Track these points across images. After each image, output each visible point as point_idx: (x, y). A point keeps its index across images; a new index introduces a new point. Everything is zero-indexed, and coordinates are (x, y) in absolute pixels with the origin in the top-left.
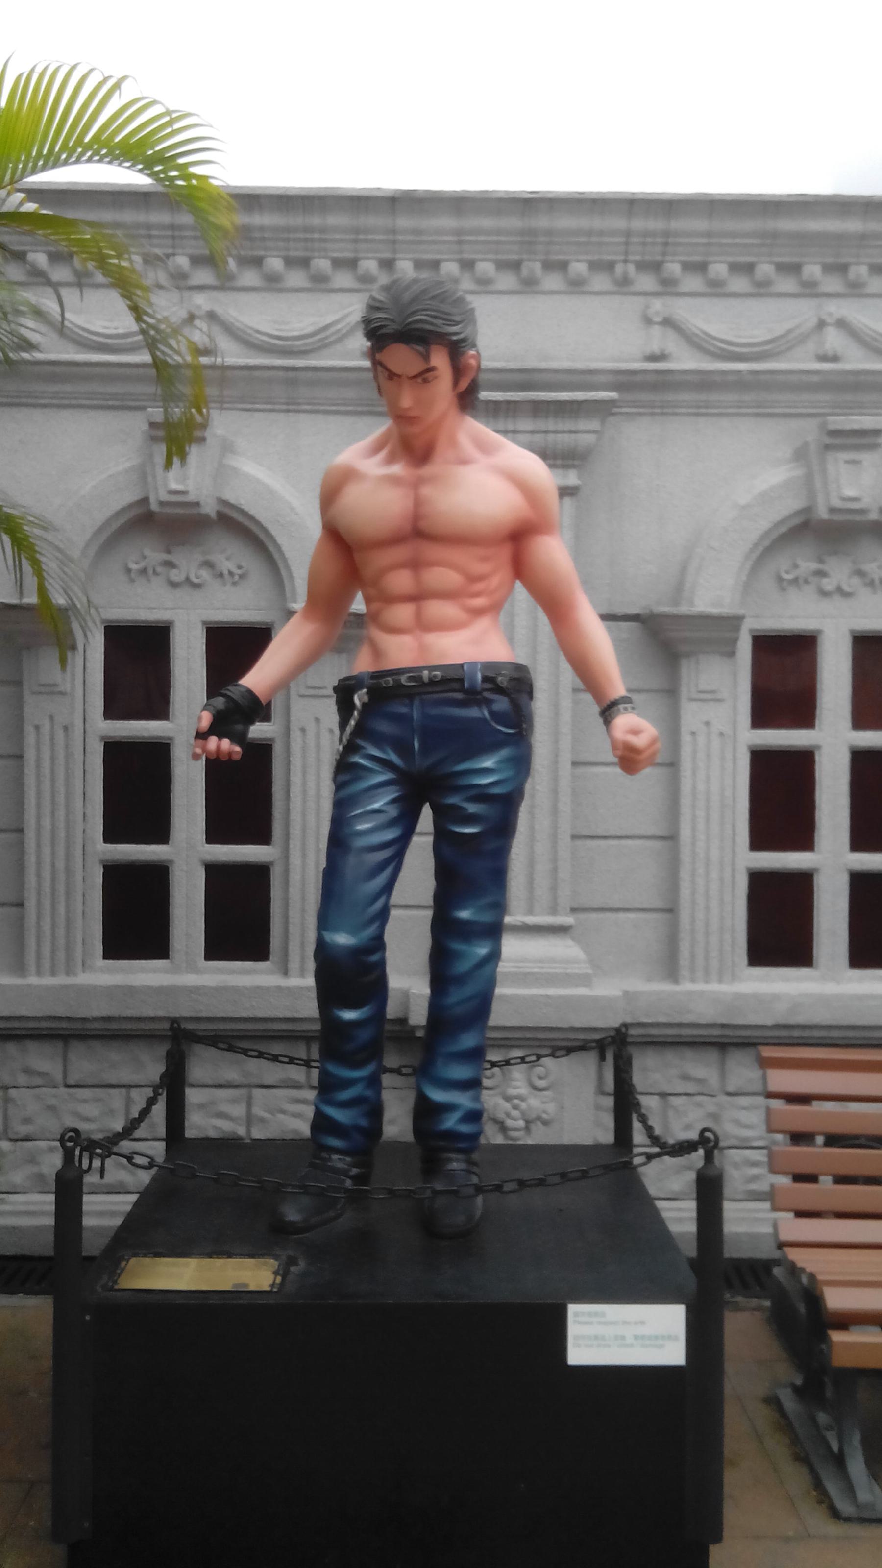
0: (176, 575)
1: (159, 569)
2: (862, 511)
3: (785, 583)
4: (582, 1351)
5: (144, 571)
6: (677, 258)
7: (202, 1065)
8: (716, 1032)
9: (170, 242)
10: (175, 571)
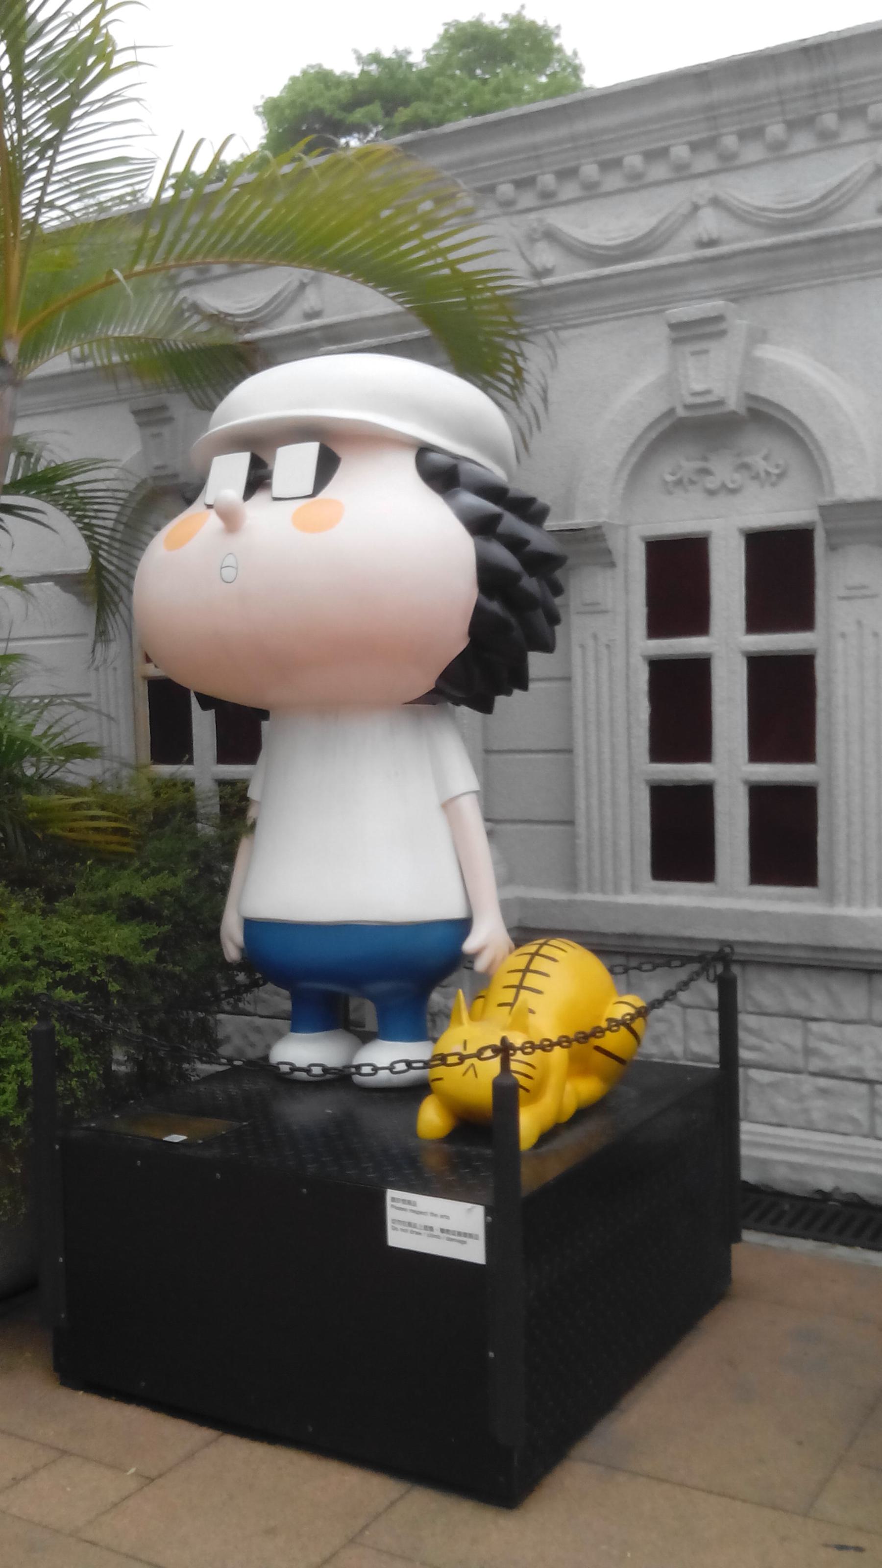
0: (711, 483)
1: (695, 478)
4: (396, 1239)
5: (679, 483)
7: (757, 991)
8: (675, 945)
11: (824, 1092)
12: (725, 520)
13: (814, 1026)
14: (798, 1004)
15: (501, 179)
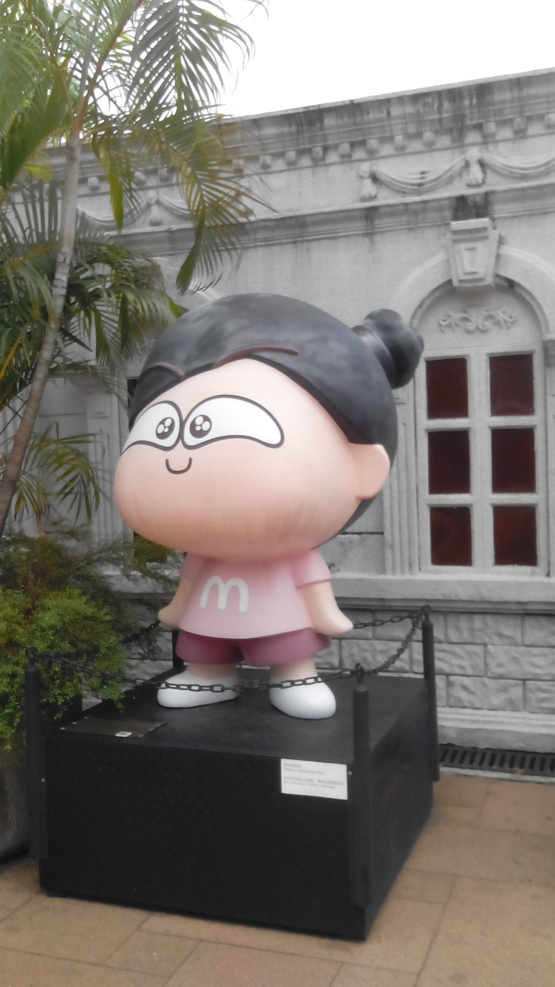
0: (471, 326)
1: (459, 323)
2: (482, 280)
4: (289, 787)
5: (449, 326)
9: (546, 105)
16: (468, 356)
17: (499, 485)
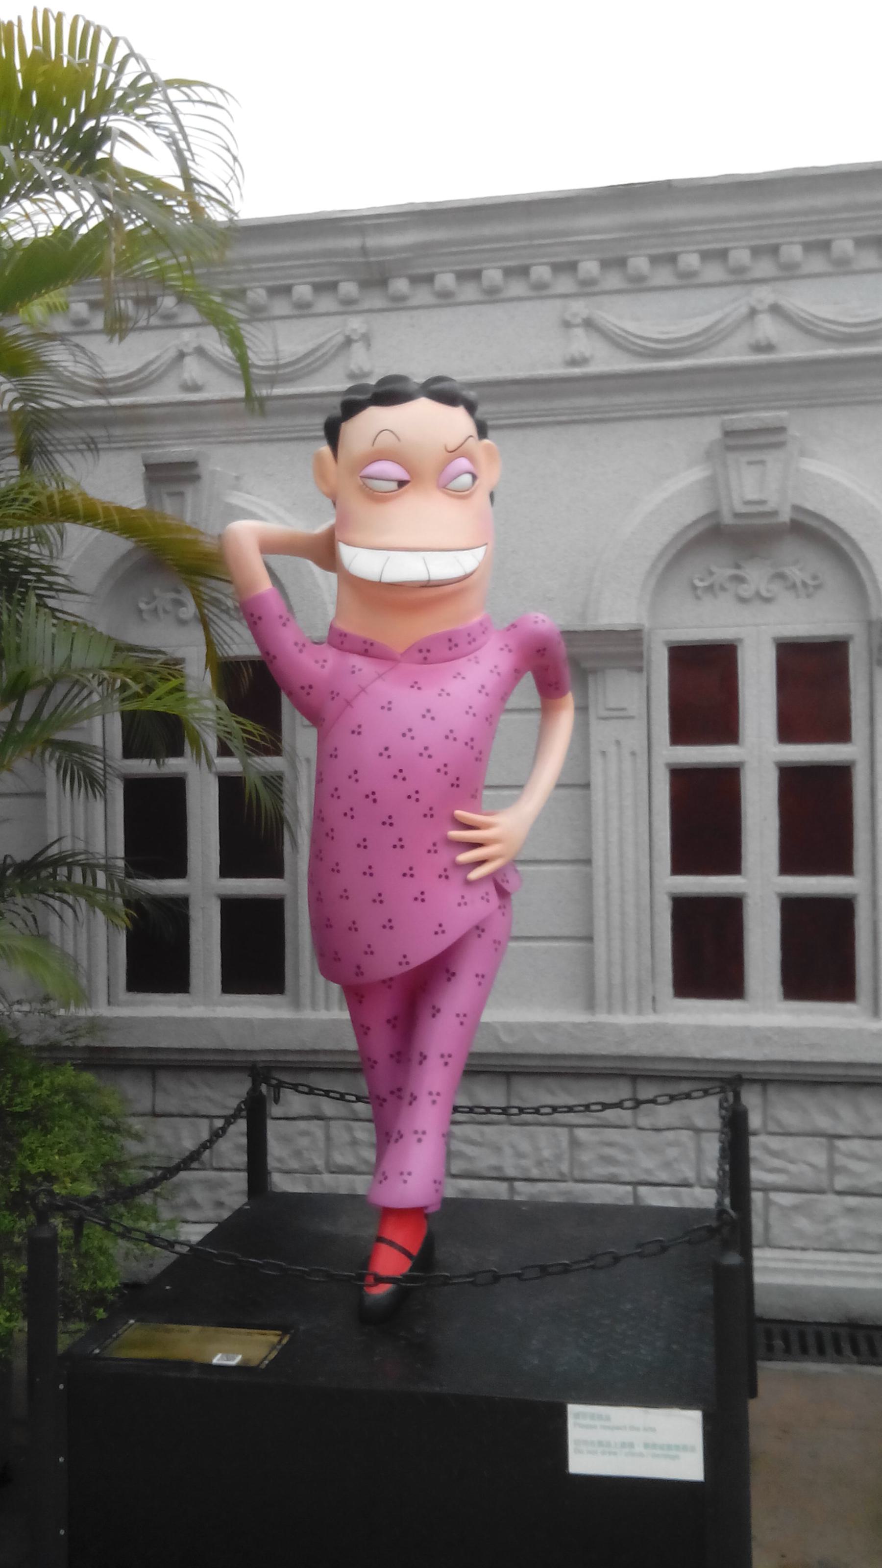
0: (746, 590)
2: (775, 513)
3: (699, 592)
4: (582, 1462)
5: (710, 588)
6: (263, 283)
10: (745, 586)
11: (850, 1211)
12: (757, 628)
13: (840, 1143)
14: (824, 1122)
15: (789, 239)
16: (740, 640)
17: (792, 861)
